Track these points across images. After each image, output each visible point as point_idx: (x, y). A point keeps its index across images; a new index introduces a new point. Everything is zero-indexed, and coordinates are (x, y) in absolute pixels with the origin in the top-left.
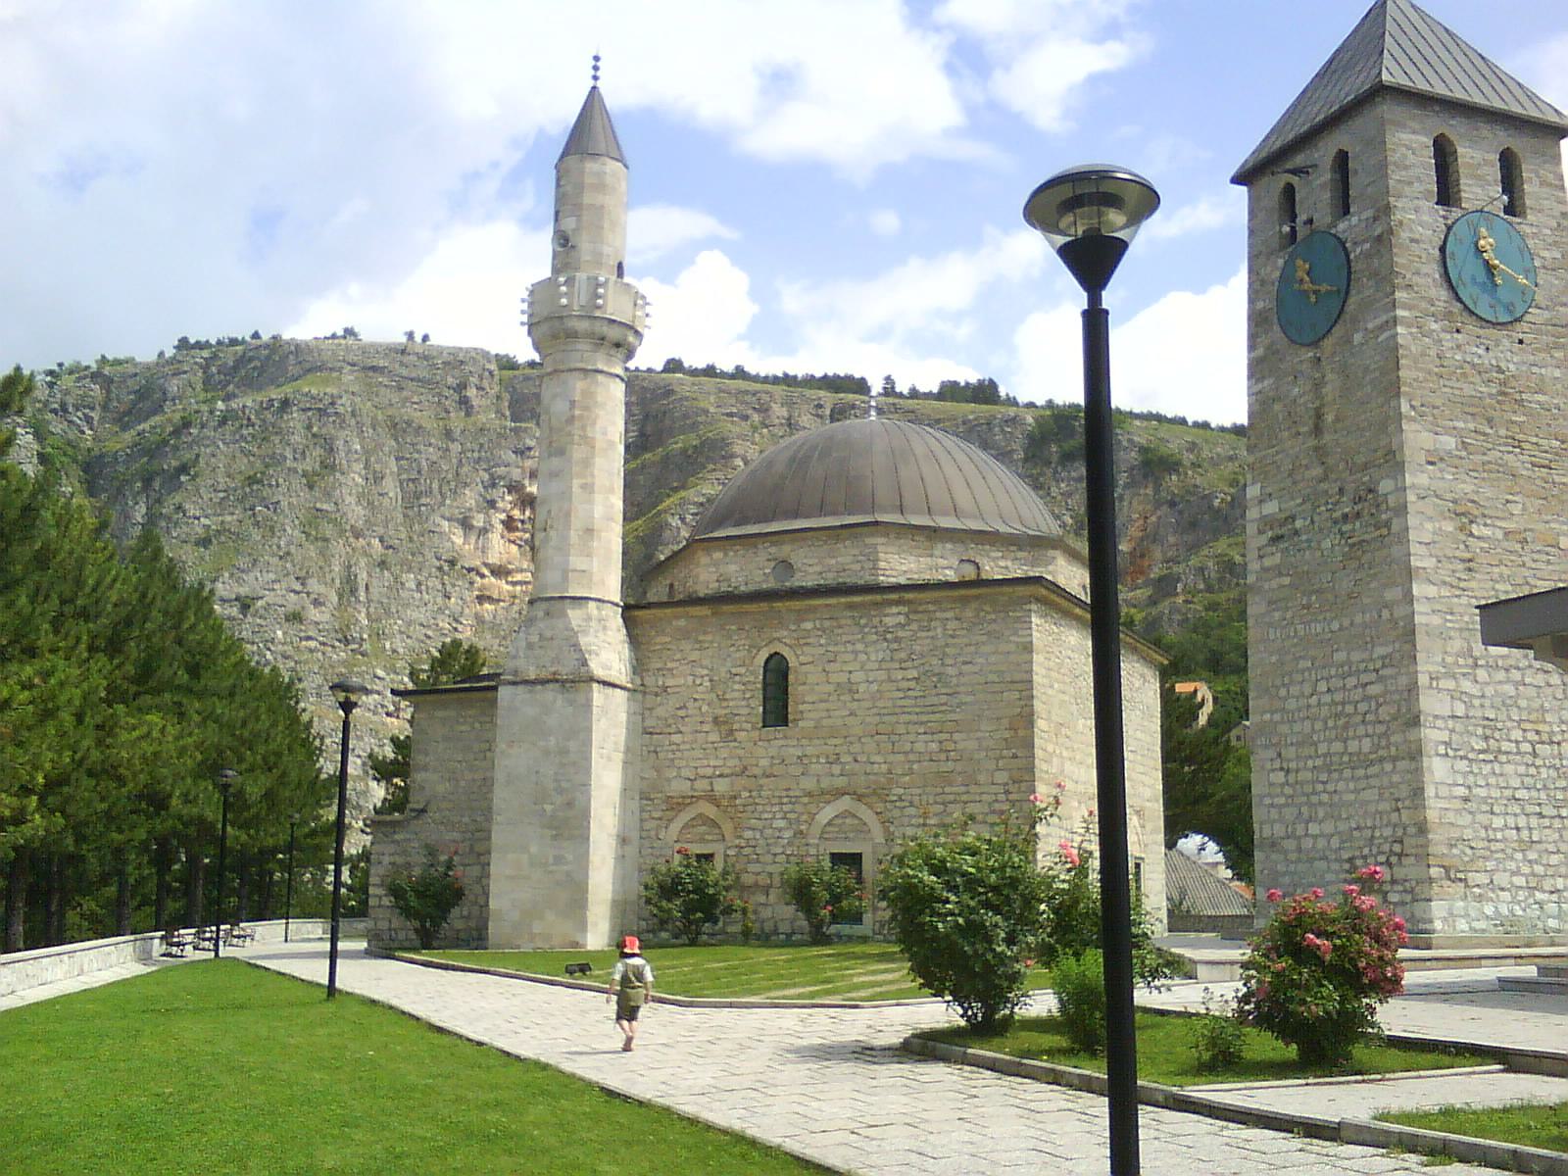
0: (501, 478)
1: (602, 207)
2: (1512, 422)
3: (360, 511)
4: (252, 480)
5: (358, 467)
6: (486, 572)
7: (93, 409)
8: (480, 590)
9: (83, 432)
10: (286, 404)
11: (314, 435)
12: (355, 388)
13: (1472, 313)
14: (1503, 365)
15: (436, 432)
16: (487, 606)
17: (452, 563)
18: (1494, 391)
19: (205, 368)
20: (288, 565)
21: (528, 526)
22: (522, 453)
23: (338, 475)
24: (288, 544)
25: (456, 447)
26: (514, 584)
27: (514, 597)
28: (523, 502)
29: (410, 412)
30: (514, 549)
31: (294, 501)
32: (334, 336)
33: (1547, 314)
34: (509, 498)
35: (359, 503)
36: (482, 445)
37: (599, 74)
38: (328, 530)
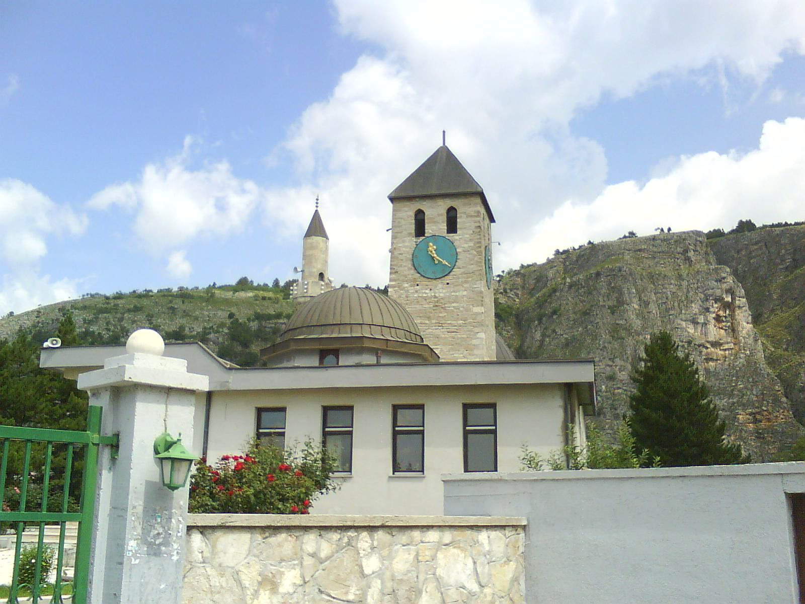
0: (710, 295)
1: (312, 255)
2: (439, 316)
3: (639, 322)
4: (585, 313)
5: (635, 300)
6: (709, 346)
7: (518, 289)
8: (706, 355)
9: (515, 301)
10: (598, 274)
11: (613, 288)
12: (631, 262)
13: (424, 277)
14: (437, 295)
15: (674, 277)
16: (711, 363)
17: (689, 342)
18: (432, 306)
19: (564, 263)
20: (605, 353)
21: (729, 319)
22: (720, 281)
23: (625, 306)
24: (604, 343)
25: (685, 283)
26: (725, 350)
27: (726, 357)
28: (724, 307)
29: (660, 269)
30: (722, 331)
31: (605, 321)
32: (625, 237)
33: (462, 270)
34: (715, 305)
35: (637, 318)
36: (698, 280)
37: (318, 205)
38: (623, 334)
